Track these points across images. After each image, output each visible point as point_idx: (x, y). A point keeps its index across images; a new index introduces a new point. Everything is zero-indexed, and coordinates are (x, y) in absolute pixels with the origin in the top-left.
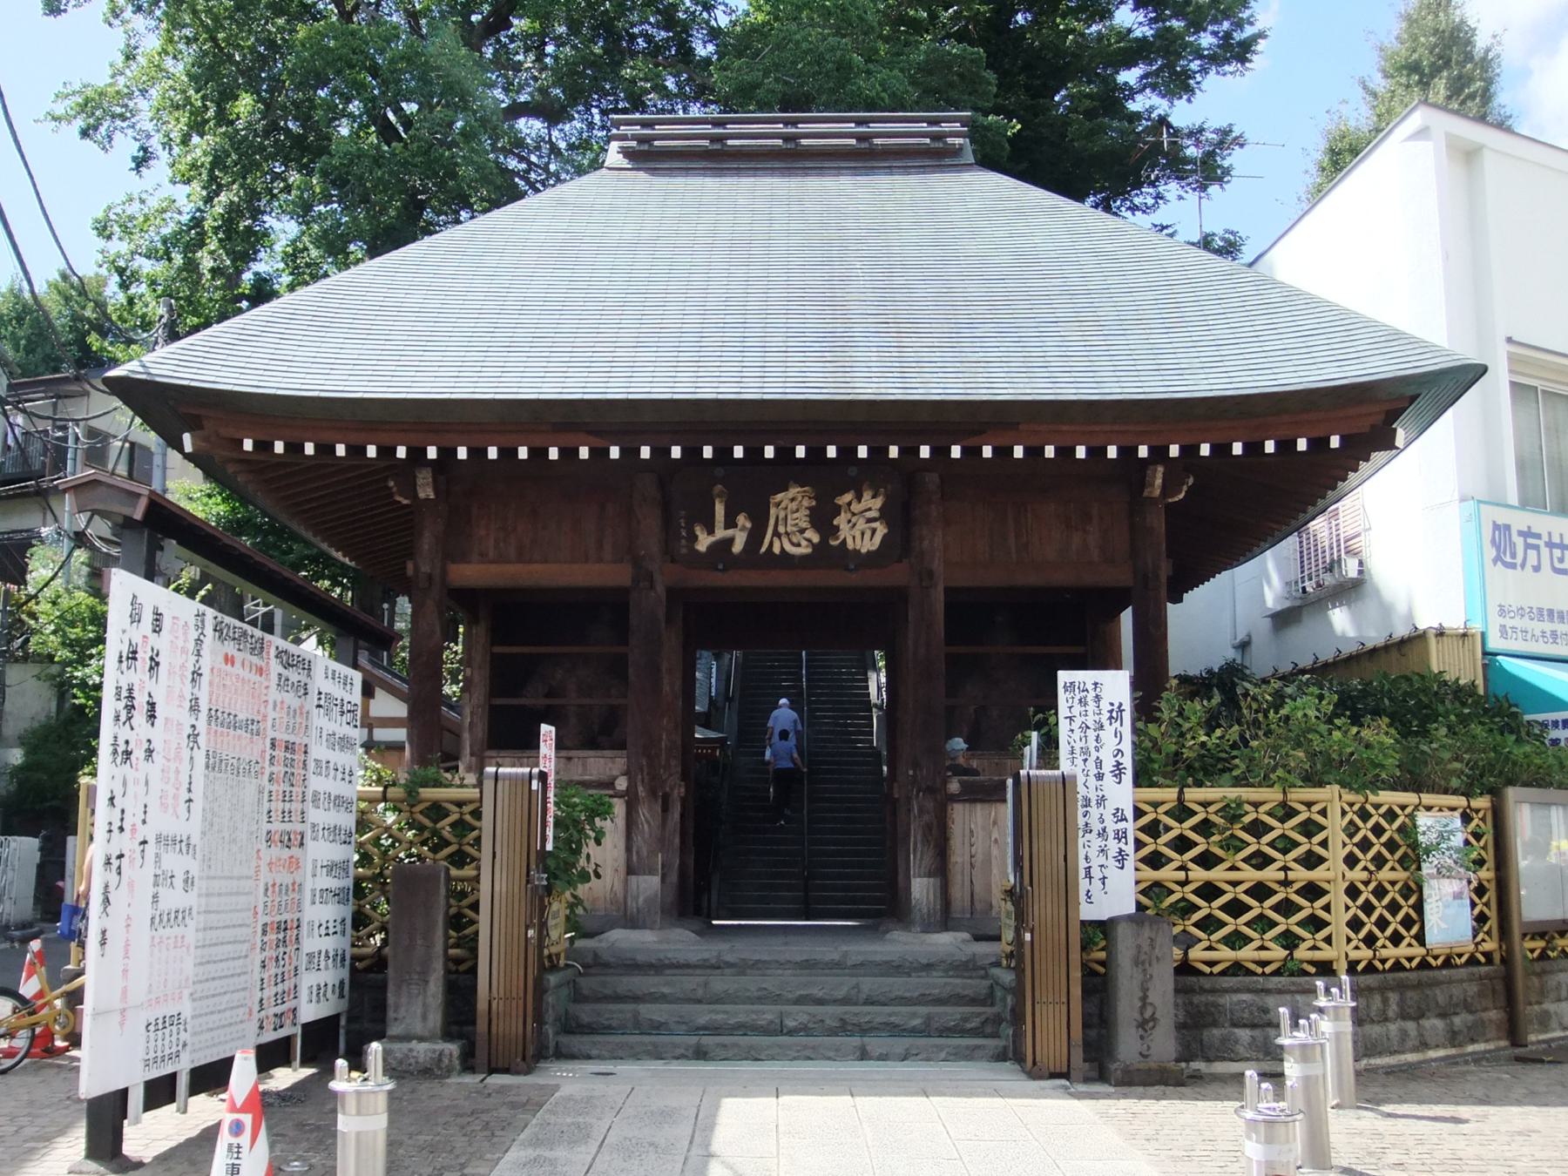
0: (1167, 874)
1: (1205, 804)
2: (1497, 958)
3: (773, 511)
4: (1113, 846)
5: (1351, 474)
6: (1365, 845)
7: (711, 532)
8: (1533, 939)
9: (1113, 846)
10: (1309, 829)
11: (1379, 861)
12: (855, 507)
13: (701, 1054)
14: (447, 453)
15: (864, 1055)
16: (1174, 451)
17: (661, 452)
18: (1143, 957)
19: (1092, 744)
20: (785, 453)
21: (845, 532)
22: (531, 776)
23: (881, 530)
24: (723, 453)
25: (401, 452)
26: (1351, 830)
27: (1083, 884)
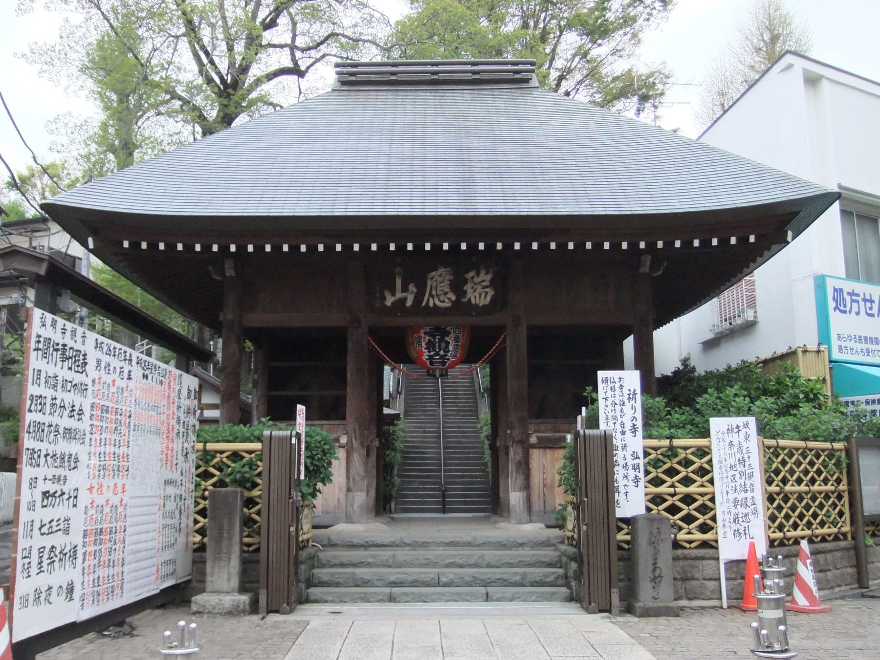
0: (663, 489)
1: (686, 448)
3: (429, 282)
4: (632, 474)
6: (777, 472)
7: (394, 294)
9: (632, 474)
12: (476, 280)
13: (392, 599)
14: (242, 248)
15: (488, 598)
18: (653, 540)
19: (618, 414)
22: (291, 436)
23: (491, 293)
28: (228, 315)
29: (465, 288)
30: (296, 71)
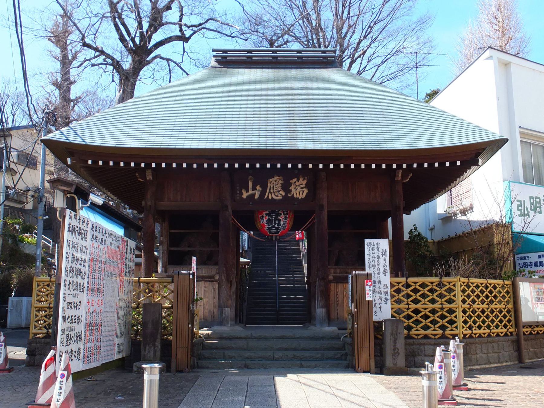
0: (403, 306)
2: (514, 334)
3: (269, 184)
4: (383, 297)
5: (465, 173)
6: (469, 296)
7: (248, 191)
8: (527, 328)
9: (383, 297)
10: (450, 290)
11: (474, 301)
12: (297, 183)
13: (247, 367)
16: (405, 166)
17: (231, 166)
19: (376, 263)
20: (274, 166)
21: (293, 191)
23: (306, 191)
24: (253, 166)
25: (143, 165)
26: (464, 291)
27: (374, 309)
28: (148, 201)
30: (184, 39)
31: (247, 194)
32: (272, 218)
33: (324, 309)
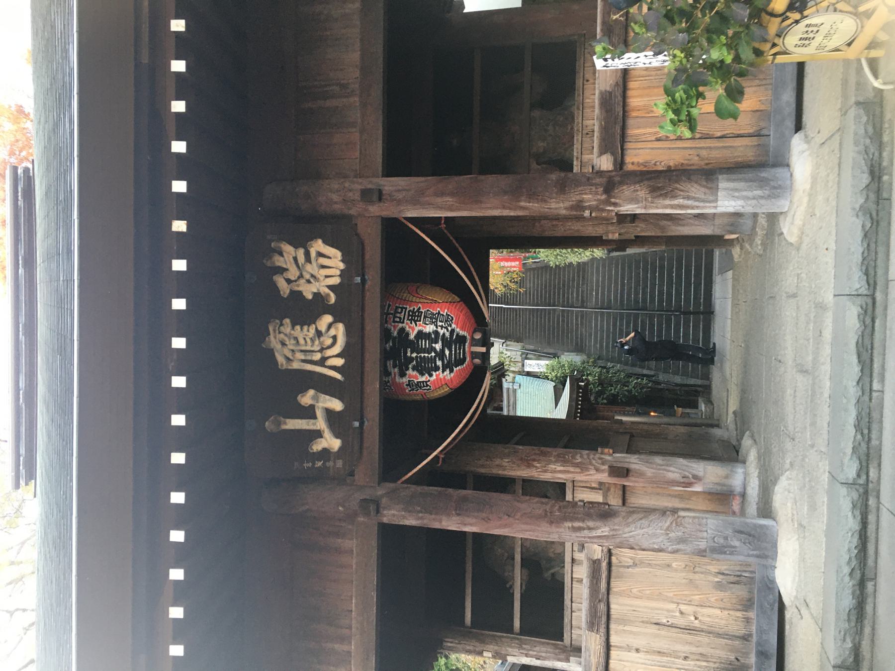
3: (296, 365)
7: (318, 434)
12: (293, 273)
23: (318, 246)
29: (310, 297)
31: (327, 434)
32: (412, 359)
33: (722, 185)
